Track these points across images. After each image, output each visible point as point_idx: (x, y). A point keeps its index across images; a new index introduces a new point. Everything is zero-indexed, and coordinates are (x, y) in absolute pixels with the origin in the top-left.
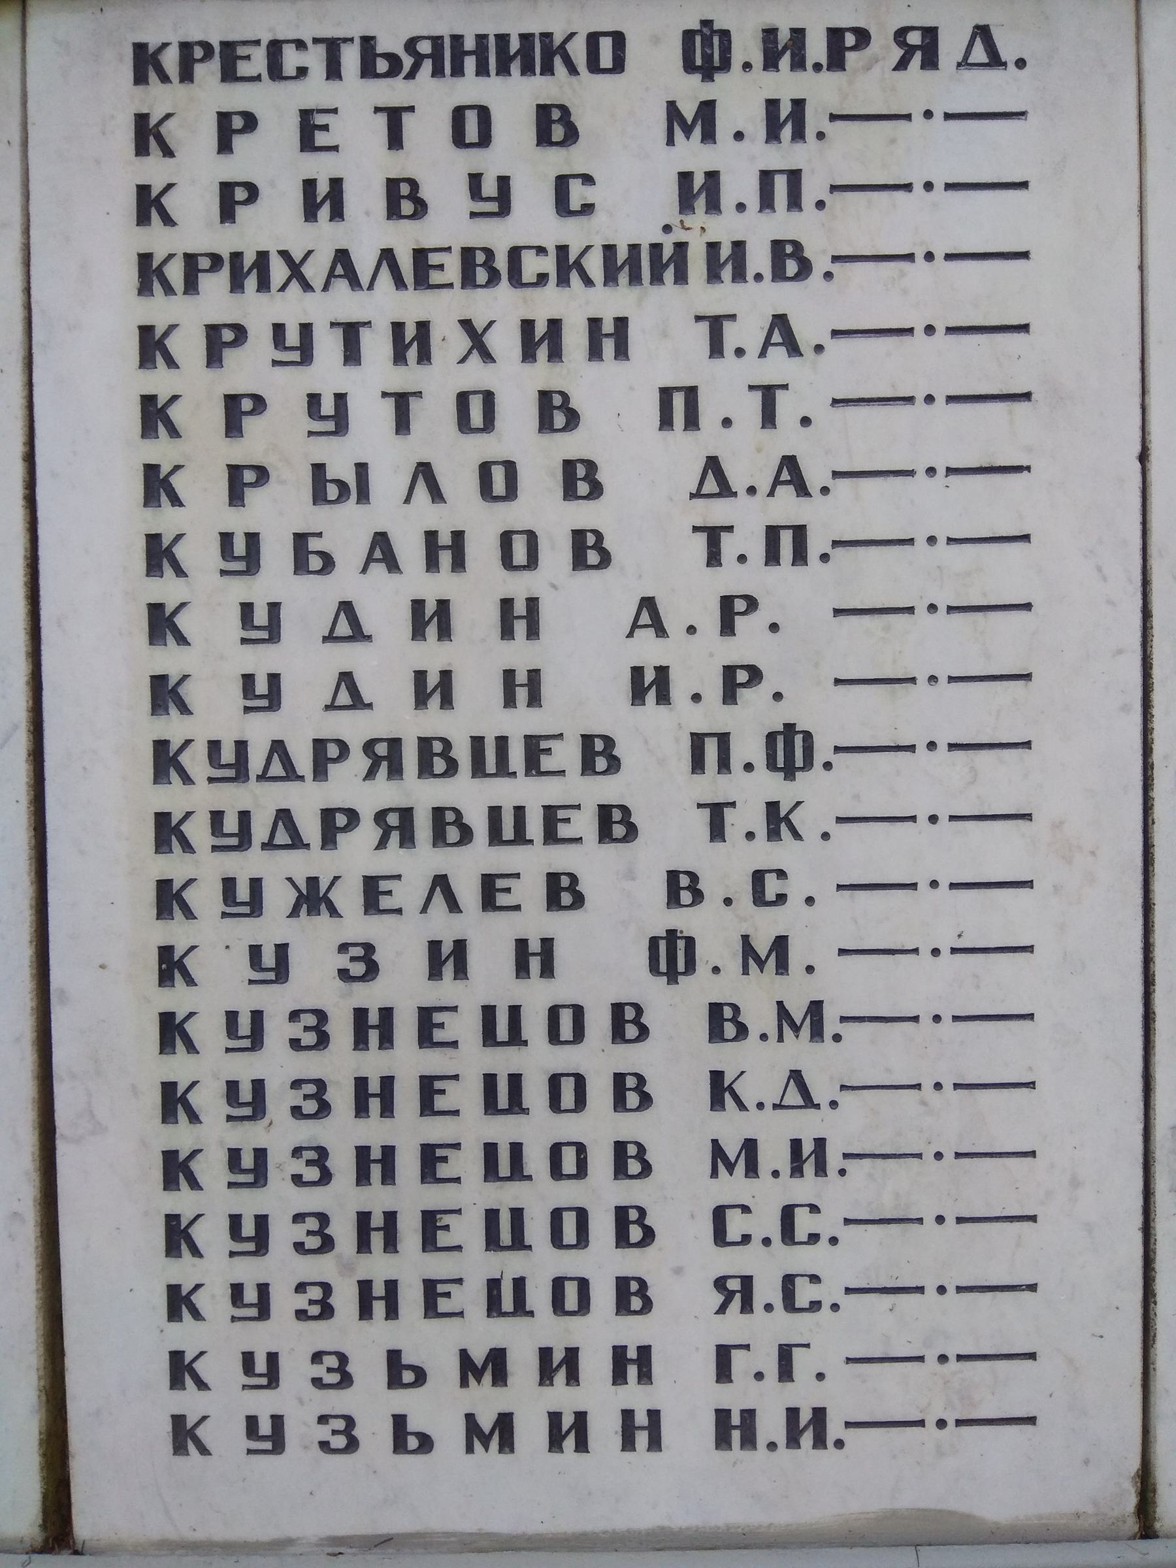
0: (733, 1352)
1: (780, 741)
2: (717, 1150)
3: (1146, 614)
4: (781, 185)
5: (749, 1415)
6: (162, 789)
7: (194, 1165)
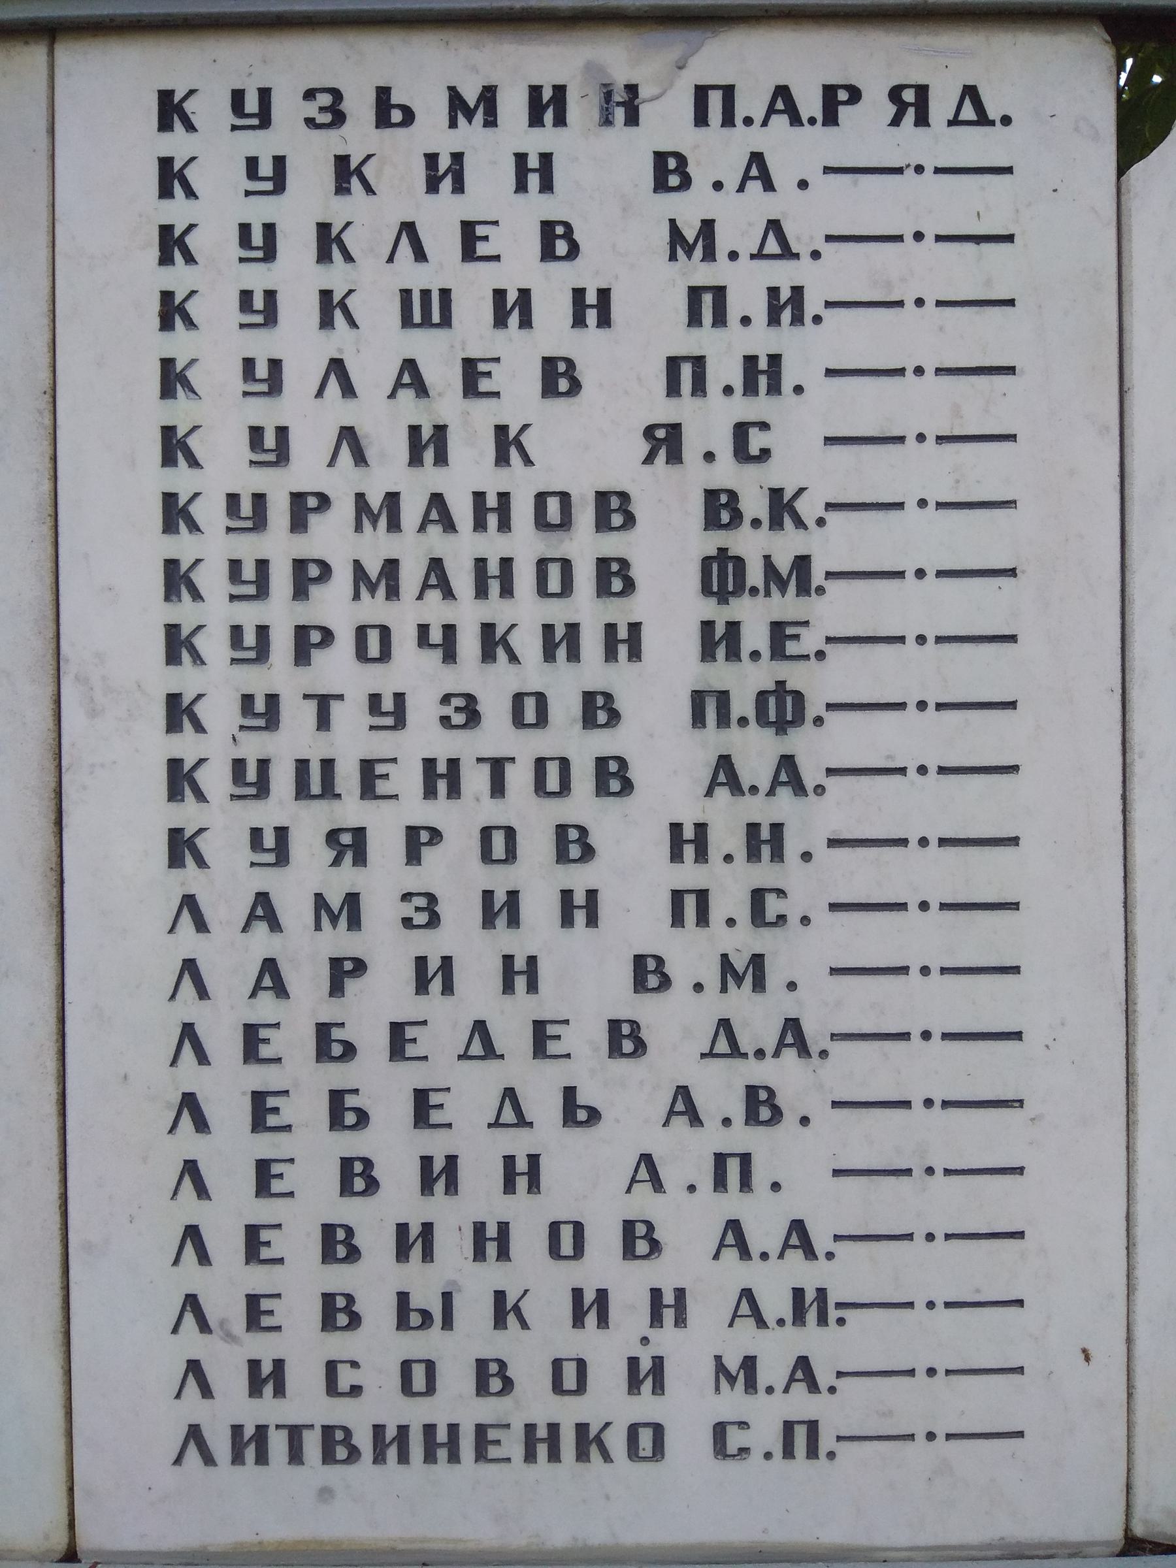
1: (772, 701)
6: (166, 136)
7: (200, 842)
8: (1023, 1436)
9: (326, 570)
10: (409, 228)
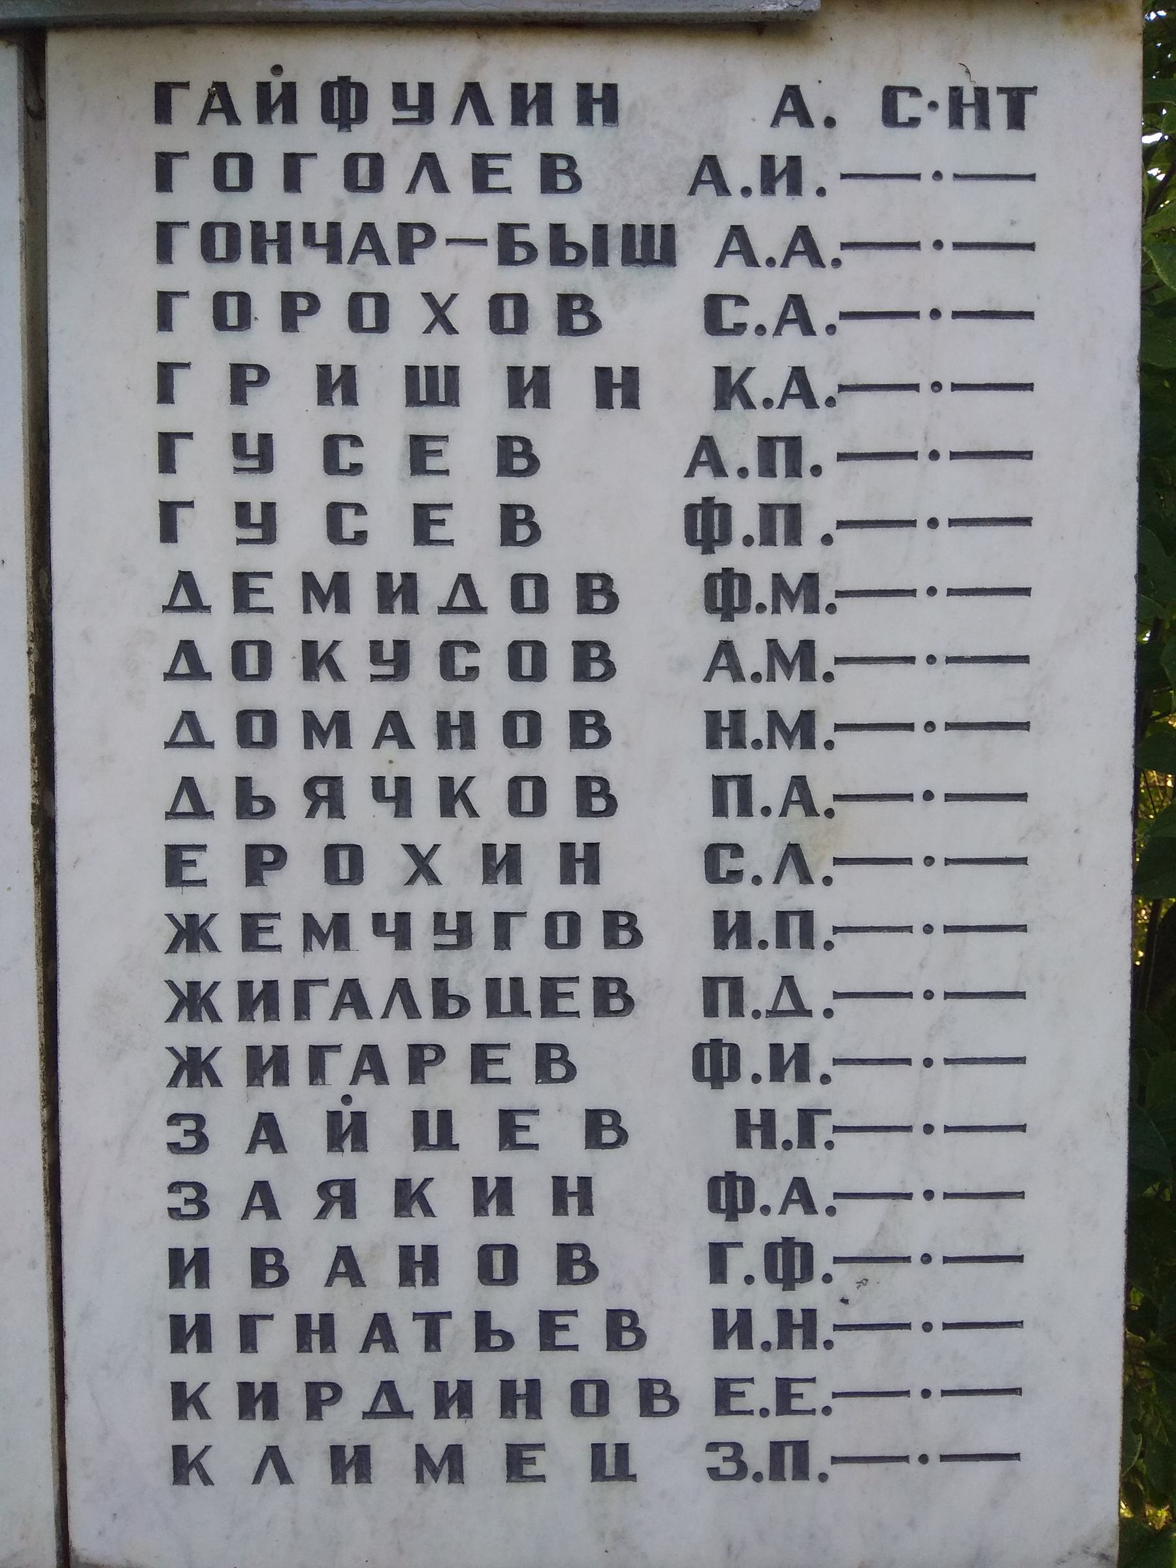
0: (728, 1250)
3: (881, 1062)
5: (738, 716)
9: (314, 304)
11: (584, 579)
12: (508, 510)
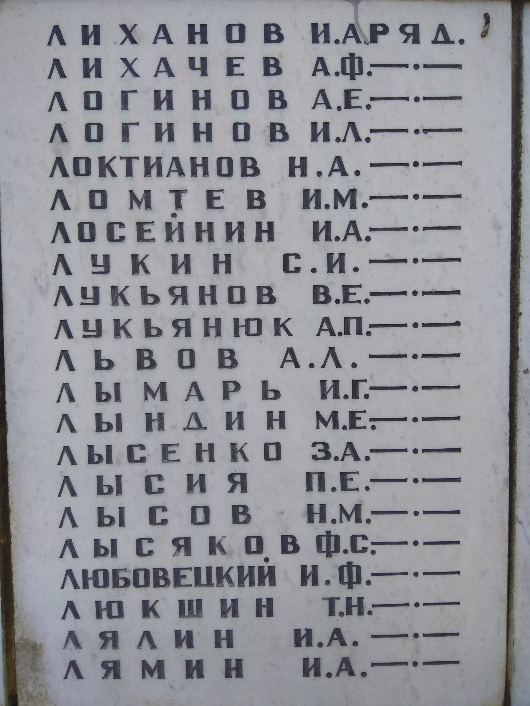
2: (319, 417)
4: (353, 324)
8: (458, 635)
10: (67, 449)
11: (259, 289)
12: (235, 508)
